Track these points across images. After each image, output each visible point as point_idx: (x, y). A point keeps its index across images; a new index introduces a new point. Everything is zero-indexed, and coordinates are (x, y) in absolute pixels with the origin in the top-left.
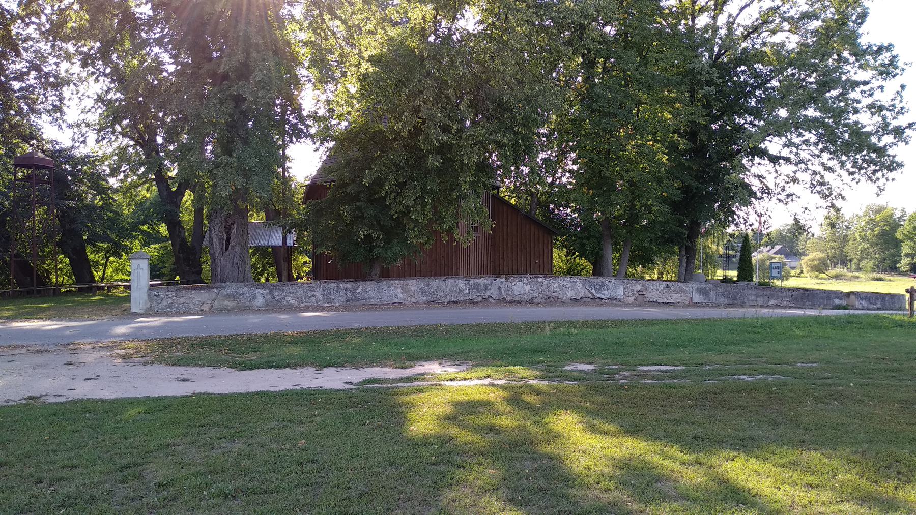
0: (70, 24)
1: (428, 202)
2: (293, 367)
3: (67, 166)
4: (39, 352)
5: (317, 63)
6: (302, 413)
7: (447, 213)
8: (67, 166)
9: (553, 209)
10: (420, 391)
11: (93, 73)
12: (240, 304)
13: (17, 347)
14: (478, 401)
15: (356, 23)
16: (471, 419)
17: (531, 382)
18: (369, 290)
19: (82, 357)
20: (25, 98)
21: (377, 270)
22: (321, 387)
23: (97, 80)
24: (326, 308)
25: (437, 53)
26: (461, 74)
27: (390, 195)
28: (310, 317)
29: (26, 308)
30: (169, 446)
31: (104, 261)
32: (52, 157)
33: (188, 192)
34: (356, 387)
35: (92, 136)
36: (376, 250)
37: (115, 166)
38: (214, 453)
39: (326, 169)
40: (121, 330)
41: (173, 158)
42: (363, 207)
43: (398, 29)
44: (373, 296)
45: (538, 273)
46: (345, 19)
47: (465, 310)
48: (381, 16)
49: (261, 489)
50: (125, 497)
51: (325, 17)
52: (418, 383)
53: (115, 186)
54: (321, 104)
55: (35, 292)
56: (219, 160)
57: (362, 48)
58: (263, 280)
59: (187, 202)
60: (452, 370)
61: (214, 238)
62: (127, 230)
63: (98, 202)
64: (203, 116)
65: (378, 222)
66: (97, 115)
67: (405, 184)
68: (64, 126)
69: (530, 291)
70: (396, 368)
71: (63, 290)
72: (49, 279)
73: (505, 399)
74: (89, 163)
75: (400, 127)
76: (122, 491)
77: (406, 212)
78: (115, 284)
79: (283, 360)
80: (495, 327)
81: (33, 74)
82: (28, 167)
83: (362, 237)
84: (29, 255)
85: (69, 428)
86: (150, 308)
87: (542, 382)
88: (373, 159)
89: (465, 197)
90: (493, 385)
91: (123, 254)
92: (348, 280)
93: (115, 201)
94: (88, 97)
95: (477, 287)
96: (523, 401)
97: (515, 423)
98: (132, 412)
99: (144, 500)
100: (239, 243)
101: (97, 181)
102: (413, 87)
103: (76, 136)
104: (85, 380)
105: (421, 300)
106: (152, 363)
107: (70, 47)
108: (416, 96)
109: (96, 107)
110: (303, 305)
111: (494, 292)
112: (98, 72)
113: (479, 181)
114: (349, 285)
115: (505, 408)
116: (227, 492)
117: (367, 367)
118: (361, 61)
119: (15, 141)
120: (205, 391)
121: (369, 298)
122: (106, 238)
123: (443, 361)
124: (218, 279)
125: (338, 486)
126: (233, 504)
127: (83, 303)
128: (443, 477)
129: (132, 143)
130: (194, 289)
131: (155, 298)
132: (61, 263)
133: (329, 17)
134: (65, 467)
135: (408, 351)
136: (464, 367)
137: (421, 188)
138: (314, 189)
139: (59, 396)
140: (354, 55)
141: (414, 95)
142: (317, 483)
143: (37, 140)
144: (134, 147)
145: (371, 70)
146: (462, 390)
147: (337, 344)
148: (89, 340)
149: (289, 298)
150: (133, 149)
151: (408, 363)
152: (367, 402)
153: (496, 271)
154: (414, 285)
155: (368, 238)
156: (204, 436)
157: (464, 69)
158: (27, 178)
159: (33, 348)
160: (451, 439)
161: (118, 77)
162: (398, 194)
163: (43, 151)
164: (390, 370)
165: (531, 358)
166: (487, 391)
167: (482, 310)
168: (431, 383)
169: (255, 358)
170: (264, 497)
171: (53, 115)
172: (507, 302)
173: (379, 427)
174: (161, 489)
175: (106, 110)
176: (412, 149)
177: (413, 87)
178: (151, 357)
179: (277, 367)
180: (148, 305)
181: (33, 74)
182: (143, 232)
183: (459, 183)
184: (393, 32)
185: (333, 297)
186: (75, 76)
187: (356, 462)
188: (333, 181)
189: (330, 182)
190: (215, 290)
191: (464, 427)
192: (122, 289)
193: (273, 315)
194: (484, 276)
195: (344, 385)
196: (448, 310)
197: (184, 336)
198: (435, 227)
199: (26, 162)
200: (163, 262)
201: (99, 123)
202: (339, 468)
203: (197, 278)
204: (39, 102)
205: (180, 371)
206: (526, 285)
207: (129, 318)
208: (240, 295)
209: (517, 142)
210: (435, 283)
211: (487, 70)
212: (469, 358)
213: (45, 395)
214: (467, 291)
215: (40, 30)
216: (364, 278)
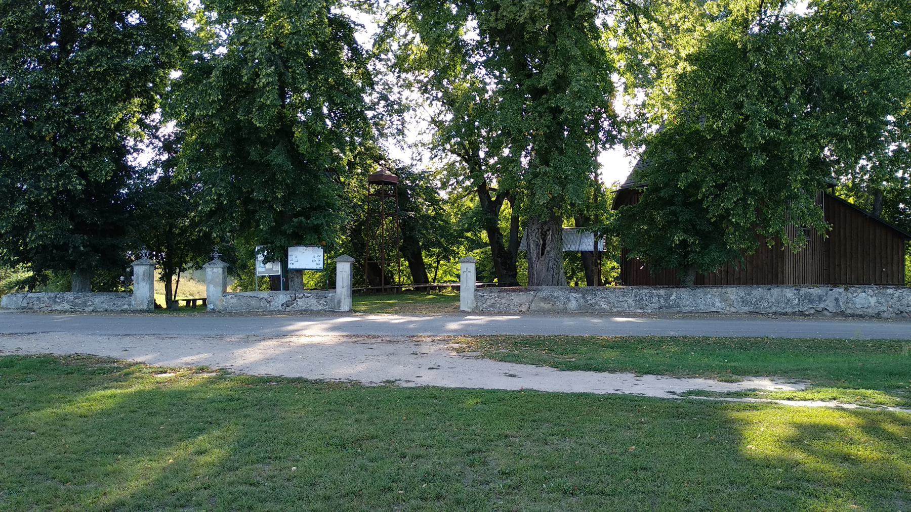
0: (412, 57)
1: (750, 204)
2: (612, 371)
3: (408, 182)
4: (390, 342)
5: (633, 67)
6: (628, 418)
7: (774, 215)
8: (408, 182)
9: (904, 209)
10: (754, 408)
11: (428, 98)
12: (555, 306)
13: (374, 337)
14: (825, 425)
15: (674, 23)
16: (818, 444)
17: (890, 409)
18: (683, 297)
19: (425, 348)
20: (376, 124)
21: (692, 277)
22: (643, 394)
23: (431, 104)
24: (638, 314)
25: (762, 43)
26: (791, 63)
27: (708, 197)
28: (623, 322)
29: (377, 303)
30: (506, 436)
31: (436, 265)
32: (396, 174)
33: (506, 201)
34: (680, 398)
35: (427, 154)
36: (691, 256)
37: (445, 180)
38: (548, 448)
39: (637, 174)
40: (453, 326)
41: (493, 169)
42: (678, 211)
43: (718, 23)
44: (687, 303)
45: (885, 283)
46: (662, 21)
47: (794, 323)
48: (700, 12)
49: (598, 489)
50: (474, 480)
51: (640, 21)
52: (750, 399)
53: (444, 198)
54: (632, 109)
55: (383, 290)
56: (538, 170)
57: (680, 47)
58: (572, 284)
59: (504, 210)
60: (787, 389)
61: (529, 242)
62: (455, 236)
63: (431, 212)
64: (524, 130)
65: (694, 227)
66: (431, 136)
67: (724, 185)
68: (405, 146)
69: (877, 304)
70: (722, 381)
71: (403, 289)
72: (393, 279)
73: (859, 426)
74: (425, 178)
75: (720, 125)
76: (470, 475)
77: (725, 216)
78: (445, 285)
79: (602, 364)
80: (833, 343)
81: (383, 103)
82: (378, 183)
83: (677, 242)
84: (377, 258)
85: (421, 411)
86: (476, 307)
87: (905, 410)
88: (689, 161)
89: (794, 197)
90: (842, 409)
91: (451, 258)
92: (662, 286)
93: (445, 211)
94: (424, 120)
95: (809, 298)
96: (884, 431)
97: (876, 455)
98: (471, 402)
99: (492, 485)
100: (554, 249)
101: (430, 193)
102: (735, 82)
103: (414, 155)
104: (429, 369)
105: (742, 309)
106: (483, 357)
107: (410, 77)
108: (738, 91)
109: (430, 128)
110: (615, 310)
111: (830, 305)
112: (432, 97)
113: (812, 179)
114: (662, 292)
115: (859, 436)
116: (565, 488)
117: (689, 378)
118: (679, 61)
119: (368, 162)
120: (531, 388)
121: (684, 306)
122: (437, 244)
123: (775, 378)
124: (534, 282)
125: (675, 497)
126: (573, 500)
127: (421, 301)
128: (794, 504)
129: (459, 159)
130: (514, 291)
131: (480, 298)
132: (402, 265)
133: (646, 20)
134: (421, 445)
135: (733, 364)
136: (802, 386)
137: (743, 189)
138: (624, 195)
139: (409, 381)
140: (671, 56)
141: (735, 90)
142: (654, 492)
143: (385, 160)
144: (460, 162)
145: (689, 69)
146: (804, 412)
147: (652, 351)
148: (429, 334)
149: (602, 303)
150: (460, 164)
151: (734, 377)
152: (696, 414)
153: (831, 279)
154: (734, 293)
155: (684, 243)
156: (537, 431)
157: (794, 58)
158: (378, 193)
159: (386, 338)
160: (798, 464)
161: (450, 102)
162: (717, 196)
163: (389, 169)
164: (714, 383)
165: (887, 381)
166: (835, 415)
167: (816, 323)
168: (765, 400)
169: (574, 359)
170: (601, 498)
171: (397, 137)
172: (846, 316)
173: (712, 442)
174: (504, 477)
175: (438, 130)
176: (736, 147)
177: (735, 82)
178: (481, 352)
179: (596, 370)
180: (475, 305)
181: (383, 103)
182: (467, 238)
183: (788, 182)
184: (711, 27)
185: (645, 303)
186: (414, 102)
187: (693, 476)
188: (645, 186)
189: (643, 187)
190: (532, 293)
191: (812, 453)
192: (450, 289)
193: (587, 319)
194: (818, 285)
195: (667, 394)
196: (774, 322)
197: (508, 334)
198: (759, 231)
199: (377, 179)
200: (484, 266)
201: (432, 143)
202: (675, 480)
203: (513, 281)
204: (386, 127)
205: (507, 367)
206: (872, 296)
207: (459, 316)
208: (555, 298)
209: (861, 134)
210: (758, 292)
211: (821, 56)
212: (806, 377)
213: (399, 380)
214: (796, 302)
215: (387, 64)
216: (678, 283)
